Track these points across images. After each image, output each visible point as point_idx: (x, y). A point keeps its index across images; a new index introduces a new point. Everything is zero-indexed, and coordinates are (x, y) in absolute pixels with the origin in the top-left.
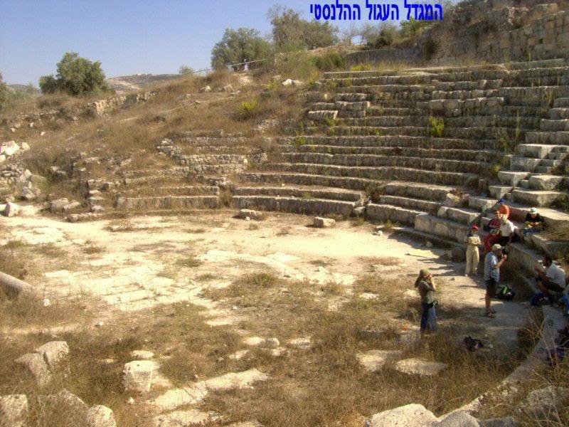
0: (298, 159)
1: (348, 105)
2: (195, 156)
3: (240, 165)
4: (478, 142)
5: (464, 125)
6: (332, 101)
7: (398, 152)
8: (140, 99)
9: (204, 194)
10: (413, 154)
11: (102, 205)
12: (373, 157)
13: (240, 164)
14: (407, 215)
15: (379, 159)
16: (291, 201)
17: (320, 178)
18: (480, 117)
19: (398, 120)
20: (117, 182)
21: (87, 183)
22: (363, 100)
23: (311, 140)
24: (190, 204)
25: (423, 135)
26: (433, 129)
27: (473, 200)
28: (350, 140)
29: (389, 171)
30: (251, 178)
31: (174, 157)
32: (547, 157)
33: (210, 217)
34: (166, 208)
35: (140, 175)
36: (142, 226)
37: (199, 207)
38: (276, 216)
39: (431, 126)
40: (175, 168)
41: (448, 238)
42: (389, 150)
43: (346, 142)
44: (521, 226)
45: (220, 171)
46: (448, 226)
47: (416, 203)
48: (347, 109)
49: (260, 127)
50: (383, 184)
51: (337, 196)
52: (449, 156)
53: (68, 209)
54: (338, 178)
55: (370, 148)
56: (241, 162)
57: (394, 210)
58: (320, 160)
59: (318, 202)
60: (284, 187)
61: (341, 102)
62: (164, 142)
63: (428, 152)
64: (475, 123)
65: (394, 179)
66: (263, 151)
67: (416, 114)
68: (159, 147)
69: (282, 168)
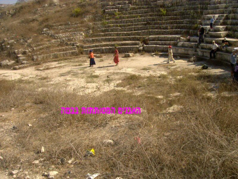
0: (105, 31)
1: (121, 7)
2: (61, 34)
3: (81, 36)
4: (182, 16)
5: (174, 11)
6: (114, 5)
7: (149, 24)
8: (8, 13)
9: (70, 50)
11: (26, 60)
12: (139, 27)
13: (81, 36)
14: (147, 48)
15: (141, 27)
16: (110, 49)
17: (118, 38)
18: (180, 7)
20: (30, 50)
21: (14, 52)
22: (127, 4)
23: (110, 22)
24: (65, 55)
25: (157, 16)
26: (162, 13)
28: (127, 21)
30: (88, 41)
31: (51, 36)
32: (217, 19)
33: (77, 60)
34: (56, 58)
35: (39, 45)
36: (54, 66)
37: (70, 56)
38: (105, 55)
40: (53, 41)
41: (185, 54)
42: (145, 23)
43: (125, 22)
44: (220, 45)
45: (74, 40)
46: (184, 49)
47: (165, 43)
48: (122, 8)
49: (85, 19)
50: (146, 37)
51: (129, 44)
52: (171, 23)
53: (10, 64)
54: (126, 37)
55: (136, 23)
56: (82, 35)
57: (157, 46)
58: (116, 30)
59: (122, 47)
60: (104, 43)
61: (118, 5)
62: (45, 30)
63: (162, 23)
64: (178, 9)
65: (151, 35)
66: (90, 29)
67: (152, 8)
68: (43, 32)
69: (100, 36)
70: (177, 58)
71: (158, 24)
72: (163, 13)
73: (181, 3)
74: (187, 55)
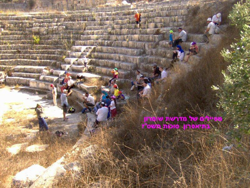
5: (48, 39)
7: (19, 52)
10: (26, 52)
12: (7, 55)
15: (10, 56)
19: (18, 37)
25: (30, 44)
26: (35, 41)
27: (55, 72)
29: (15, 61)
32: (84, 51)
39: (34, 40)
41: (45, 89)
42: (14, 51)
46: (45, 84)
47: (29, 75)
52: (43, 53)
63: (33, 52)
64: (53, 38)
70: (36, 94)
71: (30, 53)
72: (36, 41)
73: (57, 32)
74: (46, 91)
